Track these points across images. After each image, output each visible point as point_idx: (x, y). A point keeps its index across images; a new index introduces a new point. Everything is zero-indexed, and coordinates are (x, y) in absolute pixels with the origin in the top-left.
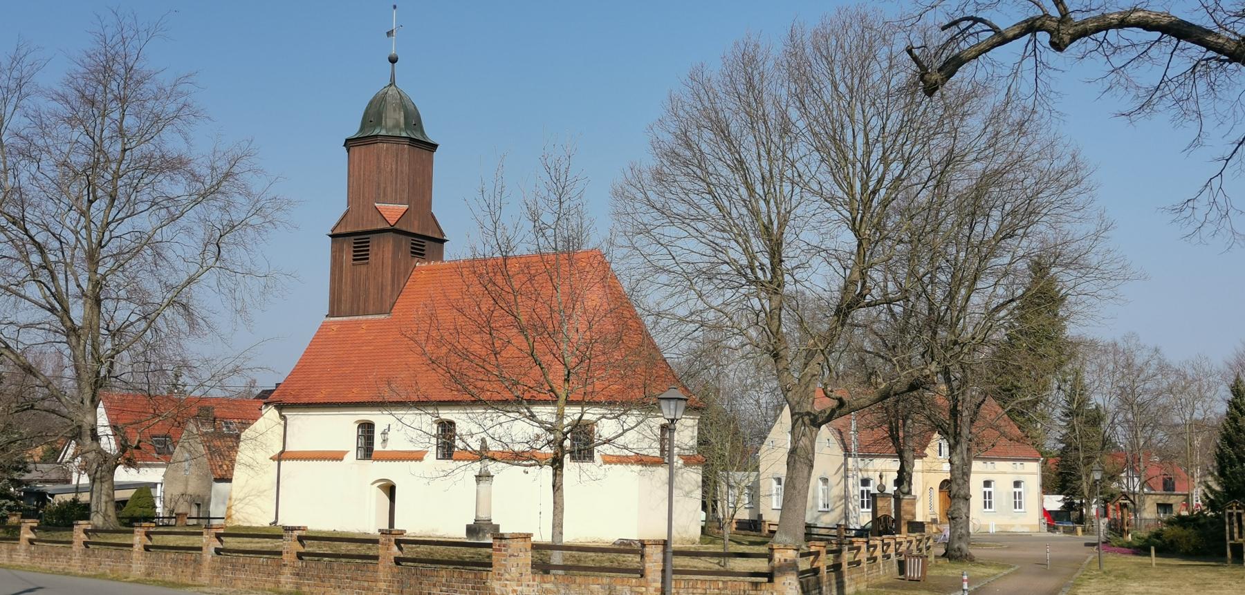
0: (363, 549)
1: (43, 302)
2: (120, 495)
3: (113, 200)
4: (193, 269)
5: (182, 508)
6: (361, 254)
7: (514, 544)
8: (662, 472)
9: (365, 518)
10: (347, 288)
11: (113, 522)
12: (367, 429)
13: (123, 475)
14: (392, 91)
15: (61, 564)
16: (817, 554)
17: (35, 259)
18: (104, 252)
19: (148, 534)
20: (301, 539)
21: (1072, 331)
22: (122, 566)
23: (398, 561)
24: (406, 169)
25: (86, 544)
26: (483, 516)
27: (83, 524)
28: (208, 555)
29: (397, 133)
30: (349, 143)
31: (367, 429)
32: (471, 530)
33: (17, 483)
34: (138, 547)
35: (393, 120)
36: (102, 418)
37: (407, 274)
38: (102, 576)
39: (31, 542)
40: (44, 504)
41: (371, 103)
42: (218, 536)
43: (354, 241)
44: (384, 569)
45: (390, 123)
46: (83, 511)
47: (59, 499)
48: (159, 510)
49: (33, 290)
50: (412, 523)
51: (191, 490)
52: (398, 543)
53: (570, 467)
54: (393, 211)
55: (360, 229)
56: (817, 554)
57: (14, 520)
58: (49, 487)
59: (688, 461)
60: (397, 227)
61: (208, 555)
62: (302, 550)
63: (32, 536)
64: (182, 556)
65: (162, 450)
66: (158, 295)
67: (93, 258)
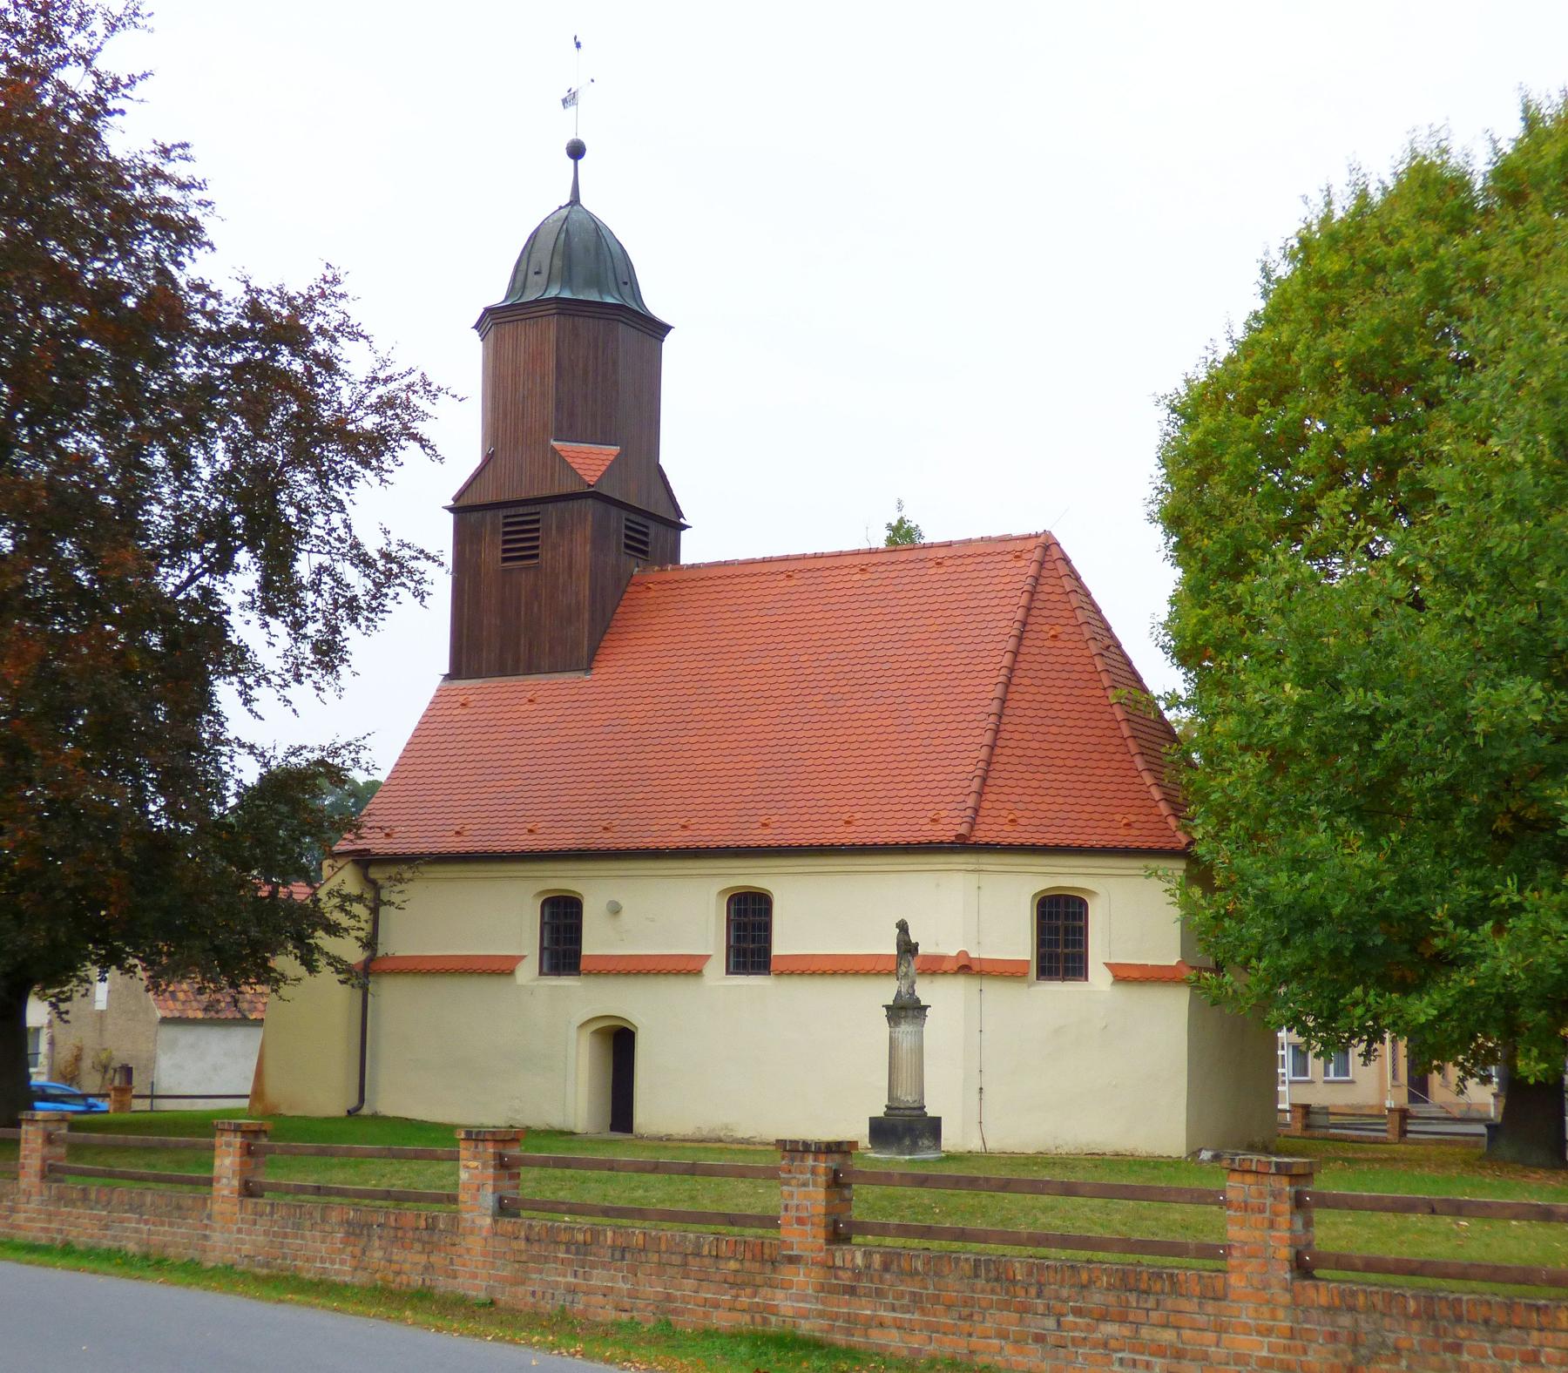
12: (562, 918)
31: (562, 918)
41: (534, 237)
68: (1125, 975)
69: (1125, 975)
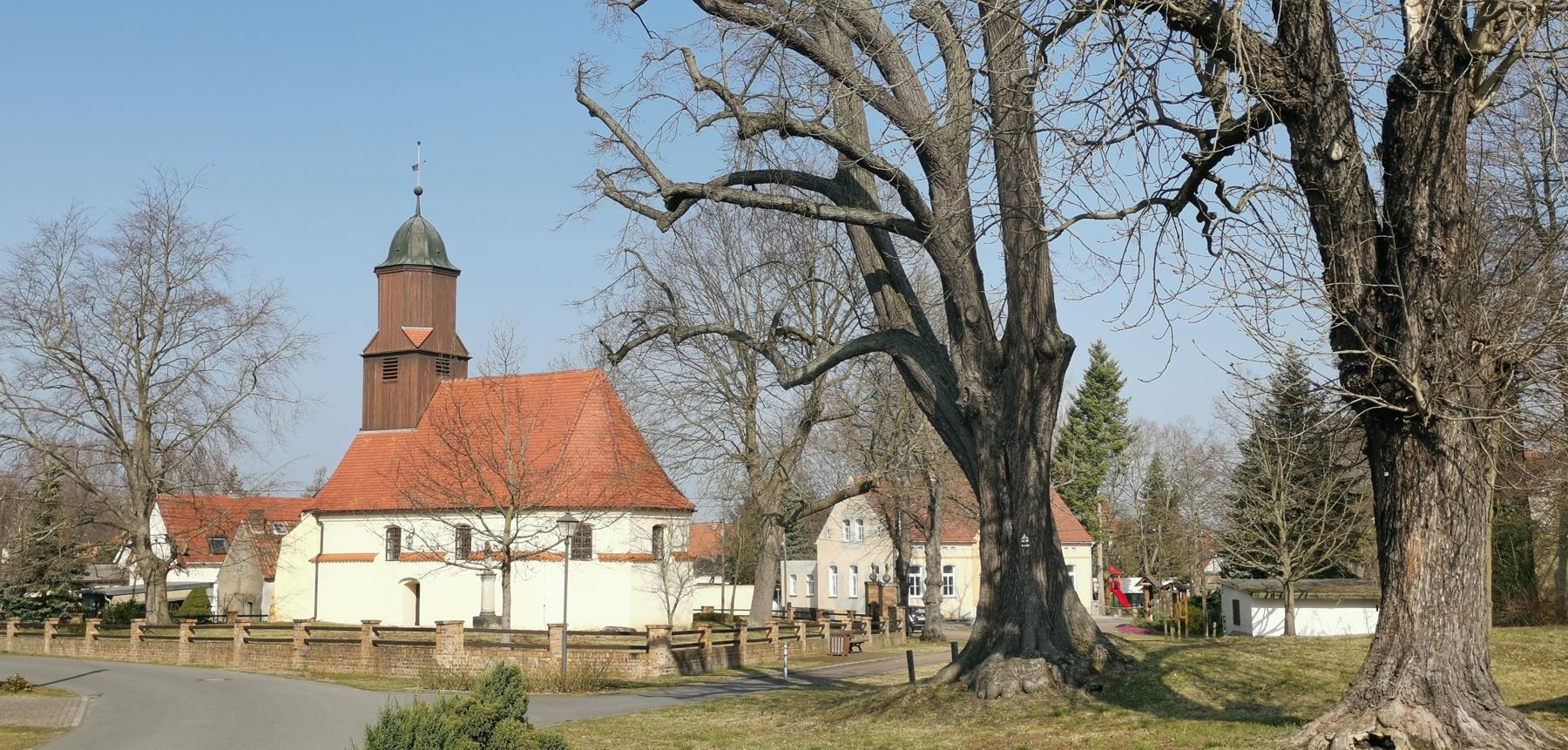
1: (100, 427)
2: (173, 596)
3: (160, 334)
4: (232, 396)
5: (235, 606)
6: (390, 373)
7: (450, 628)
8: (654, 567)
9: (396, 613)
10: (378, 405)
11: (166, 620)
12: (395, 532)
13: (173, 577)
14: (417, 222)
15: (121, 654)
16: (703, 632)
17: (91, 386)
18: (152, 381)
19: (191, 629)
20: (307, 629)
21: (1131, 418)
22: (171, 655)
23: (375, 643)
24: (430, 294)
26: (487, 609)
27: (139, 622)
28: (239, 643)
29: (421, 262)
30: (379, 270)
31: (395, 532)
32: (476, 621)
33: (77, 585)
34: (183, 639)
35: (419, 247)
36: (157, 526)
37: (434, 389)
38: (156, 663)
39: (95, 637)
40: (102, 606)
42: (246, 629)
43: (384, 361)
44: (365, 650)
45: (415, 252)
46: (141, 611)
47: (117, 600)
48: (214, 609)
49: (91, 418)
51: (243, 591)
52: (375, 630)
53: (574, 565)
54: (418, 333)
55: (389, 350)
56: (703, 632)
57: (76, 620)
58: (106, 589)
59: (679, 557)
61: (239, 643)
63: (96, 632)
64: (219, 644)
65: (217, 549)
66: (201, 419)
67: (143, 387)
68: (604, 558)
69: (604, 558)
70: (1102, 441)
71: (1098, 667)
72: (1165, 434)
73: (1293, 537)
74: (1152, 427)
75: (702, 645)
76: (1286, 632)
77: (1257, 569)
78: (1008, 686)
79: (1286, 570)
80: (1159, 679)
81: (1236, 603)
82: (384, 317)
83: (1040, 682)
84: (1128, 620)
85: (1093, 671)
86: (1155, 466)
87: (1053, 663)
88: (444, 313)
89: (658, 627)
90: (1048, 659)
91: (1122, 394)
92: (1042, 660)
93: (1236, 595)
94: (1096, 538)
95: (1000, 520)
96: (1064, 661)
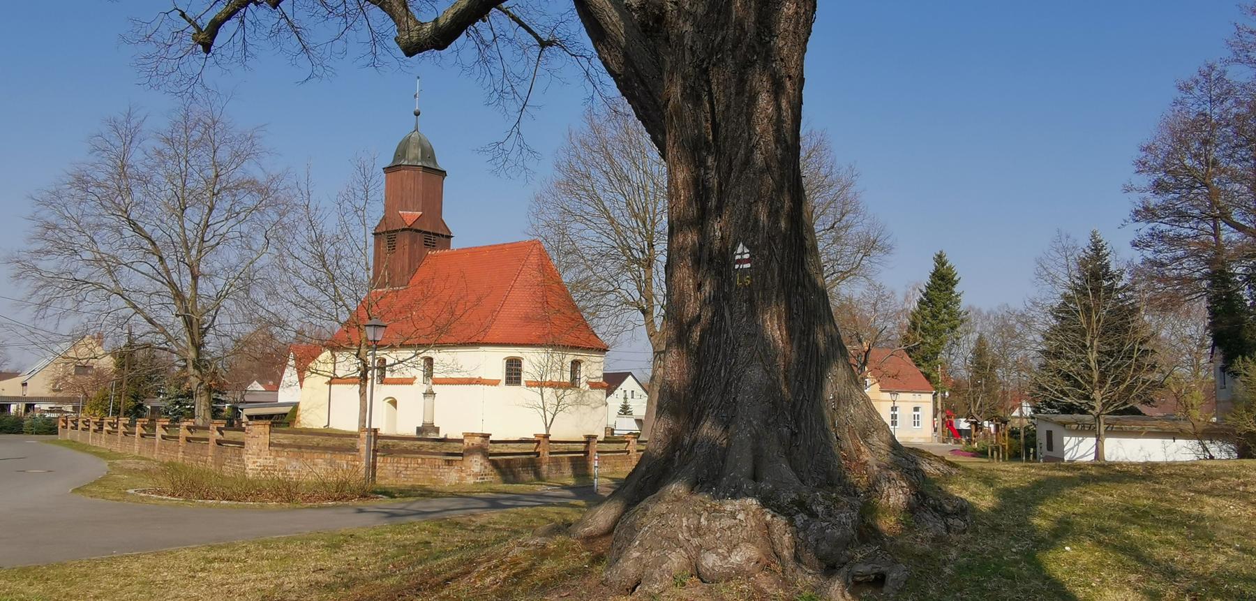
0: (348, 441)
6: (392, 247)
21: (963, 306)
24: (420, 187)
25: (125, 434)
26: (428, 421)
30: (387, 170)
32: (419, 430)
39: (142, 436)
43: (387, 235)
45: (411, 157)
50: (383, 422)
54: (411, 215)
60: (415, 227)
62: (190, 435)
70: (942, 321)
71: (887, 524)
72: (988, 318)
73: (1103, 376)
74: (979, 313)
75: (538, 454)
76: (1096, 457)
77: (1069, 409)
78: (659, 562)
79: (1098, 405)
80: (1029, 557)
81: (1049, 434)
82: (388, 208)
83: (736, 558)
84: (958, 447)
85: (867, 533)
86: (980, 340)
87: (779, 510)
88: (433, 202)
89: (473, 435)
90: (765, 502)
91: (957, 289)
92: (752, 503)
93: (1049, 427)
94: (936, 389)
95: (700, 221)
96: (802, 505)
